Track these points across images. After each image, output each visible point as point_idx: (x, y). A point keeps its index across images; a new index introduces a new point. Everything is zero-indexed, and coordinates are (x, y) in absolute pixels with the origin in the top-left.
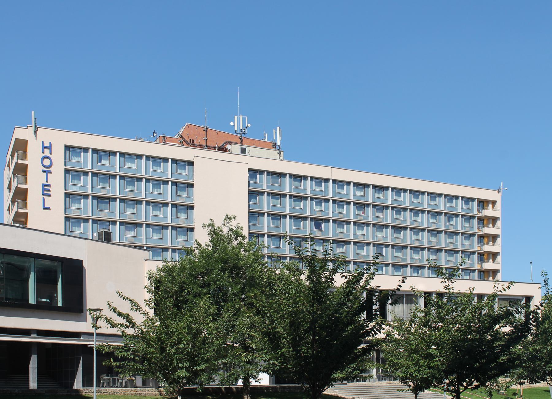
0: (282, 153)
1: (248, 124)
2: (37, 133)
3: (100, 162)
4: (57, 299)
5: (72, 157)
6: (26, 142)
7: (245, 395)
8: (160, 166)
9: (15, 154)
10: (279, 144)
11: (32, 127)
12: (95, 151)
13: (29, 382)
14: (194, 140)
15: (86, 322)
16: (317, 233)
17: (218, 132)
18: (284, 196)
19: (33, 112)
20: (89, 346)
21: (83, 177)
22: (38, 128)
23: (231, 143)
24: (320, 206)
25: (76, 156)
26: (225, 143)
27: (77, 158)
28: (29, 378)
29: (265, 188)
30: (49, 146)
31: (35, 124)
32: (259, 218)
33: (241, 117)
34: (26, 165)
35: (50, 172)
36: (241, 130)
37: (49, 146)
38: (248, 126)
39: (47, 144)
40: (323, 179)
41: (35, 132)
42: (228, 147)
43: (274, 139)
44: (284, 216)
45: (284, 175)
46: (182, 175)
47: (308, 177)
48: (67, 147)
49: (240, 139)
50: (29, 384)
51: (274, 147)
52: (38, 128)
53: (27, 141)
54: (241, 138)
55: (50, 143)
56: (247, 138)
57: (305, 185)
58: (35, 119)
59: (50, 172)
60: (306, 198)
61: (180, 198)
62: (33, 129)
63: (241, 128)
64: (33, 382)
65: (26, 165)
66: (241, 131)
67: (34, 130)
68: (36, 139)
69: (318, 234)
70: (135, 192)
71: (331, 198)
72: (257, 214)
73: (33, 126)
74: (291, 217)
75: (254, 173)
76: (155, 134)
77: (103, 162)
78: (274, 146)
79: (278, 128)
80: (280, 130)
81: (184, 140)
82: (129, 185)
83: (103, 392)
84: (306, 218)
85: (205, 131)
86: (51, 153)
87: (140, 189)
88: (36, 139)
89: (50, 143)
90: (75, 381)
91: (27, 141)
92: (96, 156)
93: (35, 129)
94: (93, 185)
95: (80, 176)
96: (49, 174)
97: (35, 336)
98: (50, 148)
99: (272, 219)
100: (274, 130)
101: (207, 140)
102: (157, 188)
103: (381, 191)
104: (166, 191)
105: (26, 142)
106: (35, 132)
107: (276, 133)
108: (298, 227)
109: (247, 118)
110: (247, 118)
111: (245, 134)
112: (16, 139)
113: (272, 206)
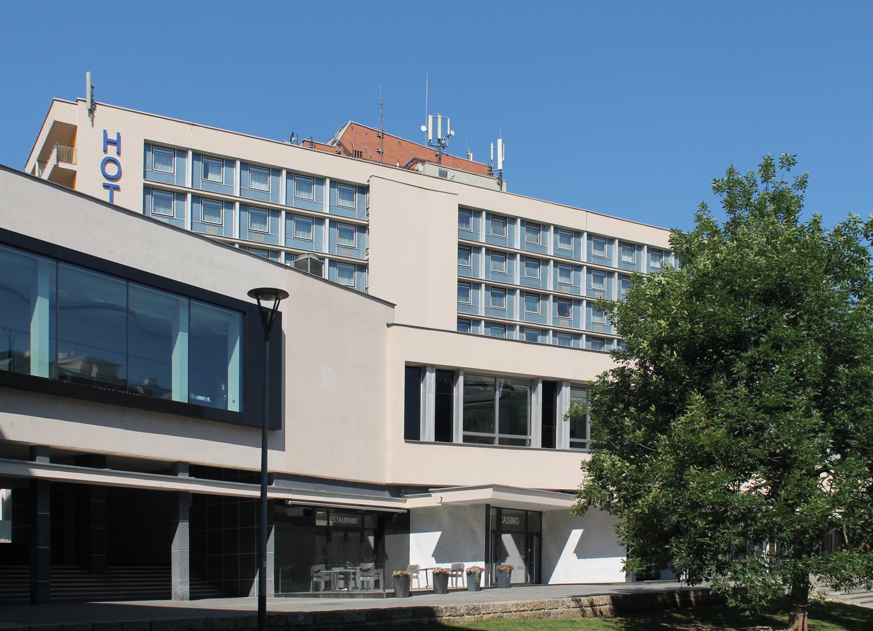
0: (504, 184)
1: (450, 131)
2: (95, 114)
3: (206, 176)
4: (227, 397)
5: (157, 165)
6: (74, 129)
7: (800, 612)
8: (310, 191)
9: (51, 152)
10: (501, 168)
11: (85, 101)
12: (198, 155)
13: (171, 581)
14: (361, 152)
15: (284, 450)
16: (561, 321)
17: (401, 141)
18: (512, 255)
19: (88, 74)
20: (290, 502)
21: (175, 203)
22: (97, 106)
23: (423, 162)
24: (567, 277)
25: (163, 164)
26: (412, 161)
27: (165, 167)
28: (171, 573)
29: (483, 239)
30: (116, 139)
31: (92, 96)
32: (471, 292)
33: (440, 117)
34: (74, 173)
35: (117, 188)
36: (439, 140)
37: (116, 139)
38: (450, 135)
39: (113, 137)
40: (572, 231)
41: (91, 111)
42: (419, 166)
43: (492, 158)
44: (512, 291)
45: (512, 219)
46: (348, 208)
47: (549, 225)
48: (149, 145)
49: (437, 156)
50: (171, 585)
51: (490, 174)
52: (97, 106)
53: (75, 128)
54: (437, 153)
55: (118, 134)
56: (448, 155)
57: (544, 239)
58: (92, 87)
59: (117, 188)
60: (546, 262)
61: (342, 249)
62: (88, 105)
63: (439, 137)
64: (182, 583)
65: (74, 173)
66: (439, 142)
67: (89, 107)
68: (93, 126)
69: (564, 324)
70: (267, 234)
71: (585, 264)
72: (469, 285)
73: (88, 99)
74: (523, 293)
75: (466, 213)
76: (293, 139)
77: (211, 177)
78: (490, 174)
79: (500, 141)
80: (502, 145)
81: (346, 151)
82: (256, 222)
83: (484, 612)
84: (546, 296)
85: (380, 137)
86: (119, 153)
87: (275, 229)
88: (93, 126)
89: (118, 134)
90: (256, 579)
91: (75, 128)
92: (200, 165)
93: (92, 106)
94: (242, 185)
95: (170, 200)
96: (115, 192)
97: (186, 476)
98: (116, 143)
99: (493, 295)
100: (492, 144)
101: (382, 153)
102: (304, 230)
103: (658, 257)
104: (319, 235)
105: (74, 129)
106: (91, 111)
107: (496, 149)
108: (532, 311)
109: (449, 120)
110: (449, 120)
111: (443, 147)
112: (55, 122)
113: (493, 272)
